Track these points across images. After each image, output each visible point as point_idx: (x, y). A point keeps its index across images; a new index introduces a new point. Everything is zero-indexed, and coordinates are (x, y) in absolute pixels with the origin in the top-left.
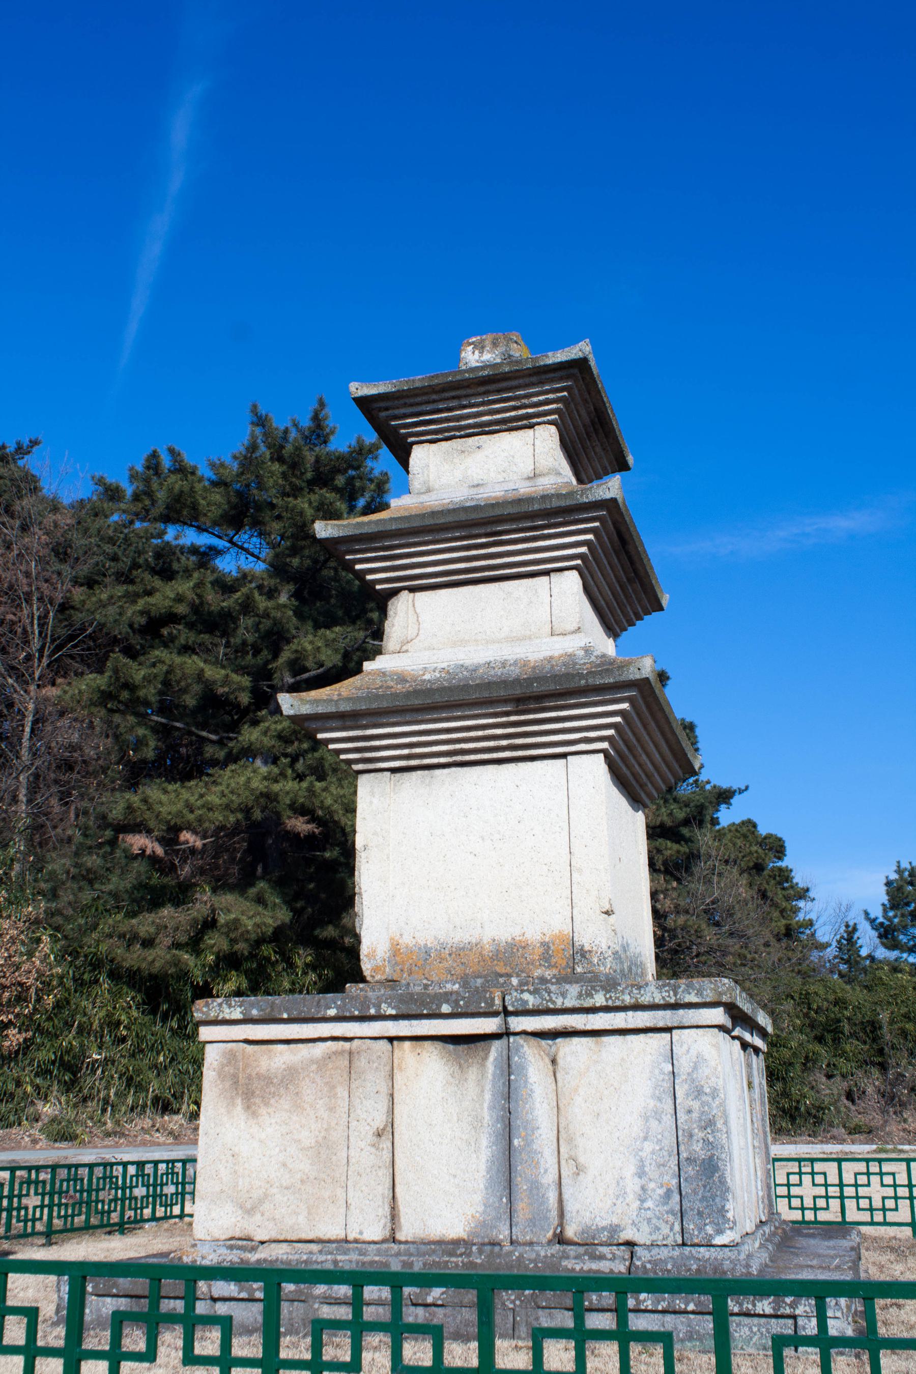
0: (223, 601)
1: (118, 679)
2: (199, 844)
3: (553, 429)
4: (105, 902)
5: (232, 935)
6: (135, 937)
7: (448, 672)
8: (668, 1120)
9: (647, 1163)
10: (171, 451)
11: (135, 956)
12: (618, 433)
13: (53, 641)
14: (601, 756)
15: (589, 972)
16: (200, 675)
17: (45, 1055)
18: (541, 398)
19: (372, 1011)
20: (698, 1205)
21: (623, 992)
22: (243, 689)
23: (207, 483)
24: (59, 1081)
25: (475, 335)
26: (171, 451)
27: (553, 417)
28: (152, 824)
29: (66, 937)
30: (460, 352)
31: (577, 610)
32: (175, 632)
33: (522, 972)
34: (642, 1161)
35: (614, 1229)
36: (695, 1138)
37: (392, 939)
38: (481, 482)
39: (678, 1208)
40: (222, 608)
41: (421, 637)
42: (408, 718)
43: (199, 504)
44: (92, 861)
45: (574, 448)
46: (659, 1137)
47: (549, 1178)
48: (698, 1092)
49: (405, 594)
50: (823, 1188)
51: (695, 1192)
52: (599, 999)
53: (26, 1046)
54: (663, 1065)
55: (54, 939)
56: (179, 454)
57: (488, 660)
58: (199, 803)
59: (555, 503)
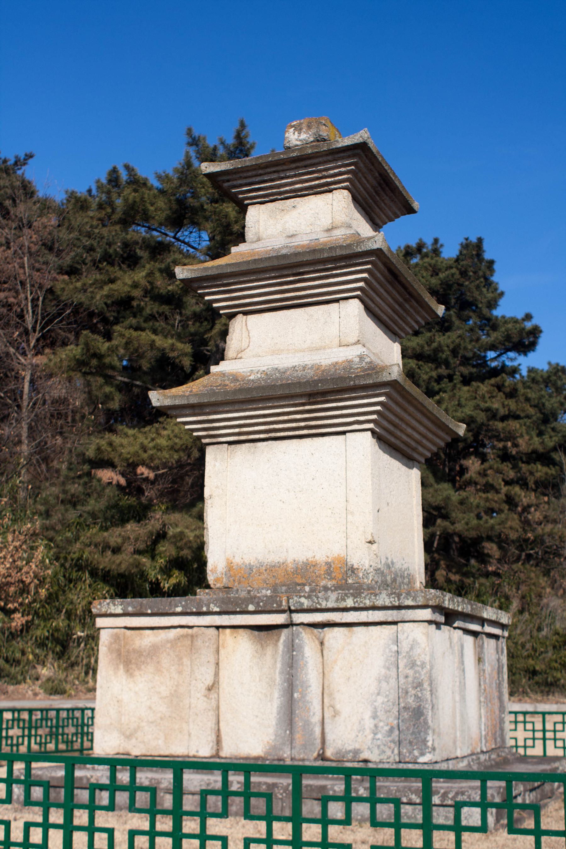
0: (169, 285)
1: (88, 350)
2: (152, 475)
3: (346, 192)
4: (85, 519)
5: (179, 544)
6: (107, 546)
7: (266, 374)
8: (393, 682)
9: (379, 710)
10: (127, 167)
11: (107, 560)
12: (401, 189)
13: (43, 319)
14: (369, 433)
15: (357, 583)
16: (152, 344)
17: (40, 632)
18: (336, 171)
19: (205, 609)
20: (409, 737)
21: (365, 598)
22: (186, 354)
23: (156, 191)
24: (53, 652)
25: (296, 120)
26: (127, 167)
27: (345, 184)
28: (116, 460)
29: (58, 546)
30: (285, 132)
31: (357, 327)
32: (142, 303)
33: (313, 582)
34: (375, 708)
35: (356, 752)
36: (409, 694)
37: (228, 559)
38: (295, 233)
39: (397, 739)
40: (169, 291)
41: (251, 347)
42: (236, 407)
43: (148, 210)
44: (75, 488)
45: (367, 203)
46: (387, 693)
47: (316, 719)
48: (413, 665)
49: (240, 316)
50: (531, 733)
51: (408, 729)
52: (350, 603)
53: (27, 627)
54: (392, 646)
55: (47, 547)
56: (133, 170)
57: (294, 364)
58: (151, 445)
59: (339, 253)
